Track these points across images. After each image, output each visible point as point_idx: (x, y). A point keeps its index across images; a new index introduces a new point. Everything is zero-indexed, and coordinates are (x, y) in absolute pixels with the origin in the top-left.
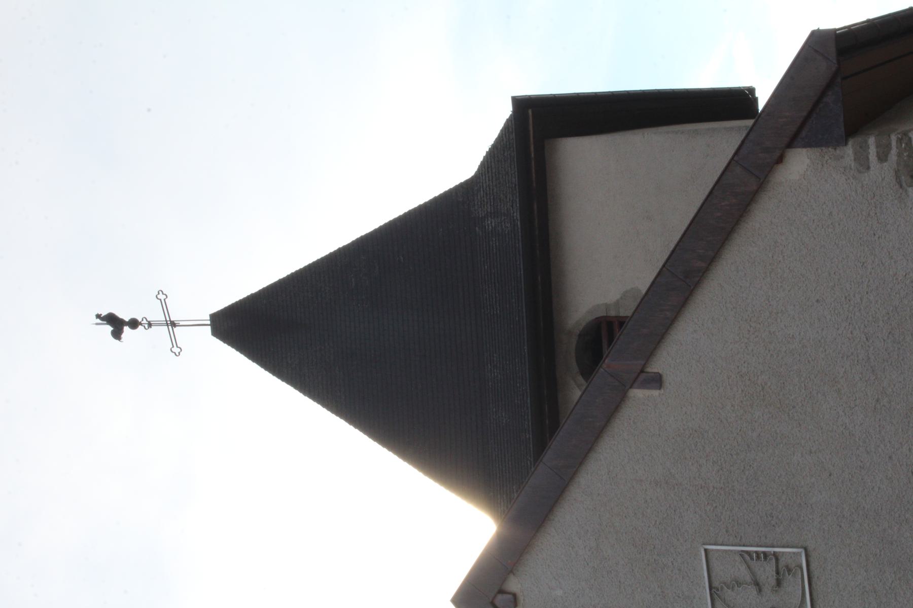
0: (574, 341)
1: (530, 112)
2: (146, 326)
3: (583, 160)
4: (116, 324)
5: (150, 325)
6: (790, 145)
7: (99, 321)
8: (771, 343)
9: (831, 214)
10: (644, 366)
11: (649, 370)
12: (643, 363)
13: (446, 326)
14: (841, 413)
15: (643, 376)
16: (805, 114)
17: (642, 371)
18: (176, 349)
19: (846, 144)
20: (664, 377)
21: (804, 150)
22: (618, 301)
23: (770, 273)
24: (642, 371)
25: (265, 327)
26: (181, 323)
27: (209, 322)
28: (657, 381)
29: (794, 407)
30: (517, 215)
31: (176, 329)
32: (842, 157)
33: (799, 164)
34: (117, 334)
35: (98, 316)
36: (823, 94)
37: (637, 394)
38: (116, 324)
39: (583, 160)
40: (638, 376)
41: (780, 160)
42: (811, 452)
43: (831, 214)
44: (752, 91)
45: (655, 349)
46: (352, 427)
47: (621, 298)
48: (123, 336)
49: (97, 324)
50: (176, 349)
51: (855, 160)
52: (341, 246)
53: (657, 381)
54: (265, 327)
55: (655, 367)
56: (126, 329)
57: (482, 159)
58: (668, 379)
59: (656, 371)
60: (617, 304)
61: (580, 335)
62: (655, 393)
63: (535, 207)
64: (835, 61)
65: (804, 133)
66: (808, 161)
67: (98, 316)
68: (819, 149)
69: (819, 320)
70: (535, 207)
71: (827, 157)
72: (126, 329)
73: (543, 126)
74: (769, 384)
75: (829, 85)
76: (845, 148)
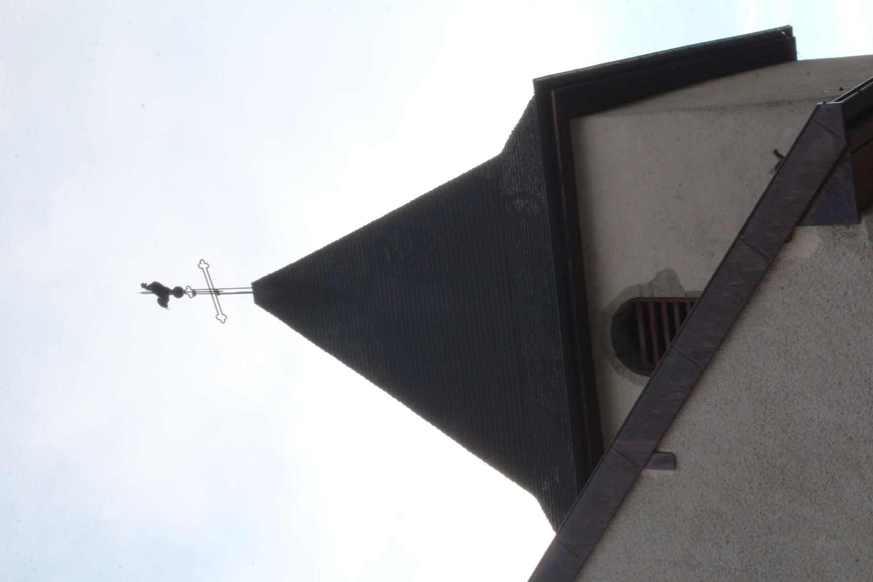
0: (609, 321)
1: (553, 93)
2: (191, 294)
3: (611, 139)
4: (161, 293)
5: (194, 293)
6: (800, 222)
7: (144, 290)
8: (788, 425)
9: (846, 294)
10: (657, 446)
11: (662, 450)
12: (655, 443)
13: (479, 301)
14: (866, 498)
15: (656, 456)
16: (813, 192)
17: (655, 451)
18: (221, 317)
19: (859, 222)
20: (679, 459)
21: (815, 227)
22: (651, 282)
23: (784, 354)
24: (655, 451)
25: (306, 295)
26: (225, 291)
27: (251, 290)
28: (671, 461)
29: (816, 491)
30: (544, 199)
31: (220, 297)
32: (856, 235)
33: (810, 242)
34: (163, 302)
35: (144, 286)
36: (832, 171)
37: (651, 474)
38: (161, 293)
39: (611, 139)
40: (651, 455)
41: (790, 238)
42: (836, 537)
43: (846, 294)
44: (788, 30)
45: (667, 429)
46: (395, 400)
47: (655, 279)
48: (169, 303)
49: (143, 293)
50: (221, 317)
51: (870, 238)
52: (374, 219)
53: (671, 461)
54: (306, 295)
55: (670, 446)
56: (172, 297)
57: (508, 138)
58: (684, 459)
59: (668, 450)
60: (651, 285)
61: (614, 317)
62: (670, 473)
63: (563, 190)
64: (843, 138)
65: (813, 211)
66: (819, 239)
67: (144, 286)
68: (830, 227)
69: (838, 402)
70: (563, 190)
71: (839, 235)
72: (172, 297)
73: (568, 104)
74: (788, 467)
75: (839, 161)
76: (858, 226)
